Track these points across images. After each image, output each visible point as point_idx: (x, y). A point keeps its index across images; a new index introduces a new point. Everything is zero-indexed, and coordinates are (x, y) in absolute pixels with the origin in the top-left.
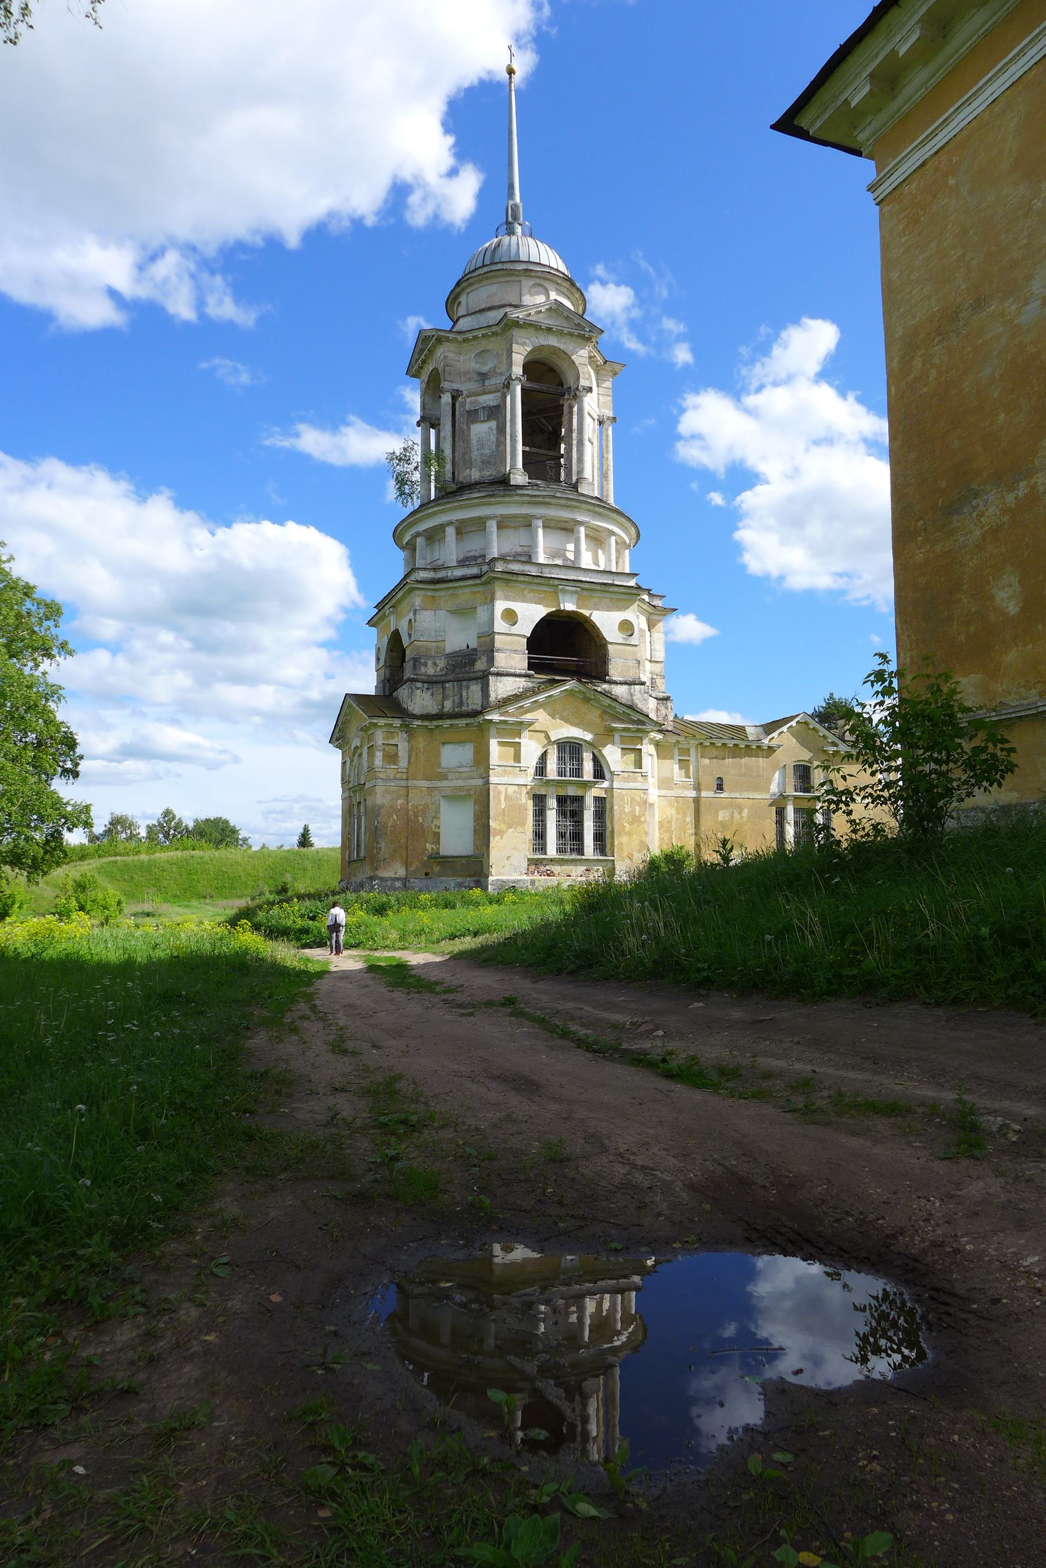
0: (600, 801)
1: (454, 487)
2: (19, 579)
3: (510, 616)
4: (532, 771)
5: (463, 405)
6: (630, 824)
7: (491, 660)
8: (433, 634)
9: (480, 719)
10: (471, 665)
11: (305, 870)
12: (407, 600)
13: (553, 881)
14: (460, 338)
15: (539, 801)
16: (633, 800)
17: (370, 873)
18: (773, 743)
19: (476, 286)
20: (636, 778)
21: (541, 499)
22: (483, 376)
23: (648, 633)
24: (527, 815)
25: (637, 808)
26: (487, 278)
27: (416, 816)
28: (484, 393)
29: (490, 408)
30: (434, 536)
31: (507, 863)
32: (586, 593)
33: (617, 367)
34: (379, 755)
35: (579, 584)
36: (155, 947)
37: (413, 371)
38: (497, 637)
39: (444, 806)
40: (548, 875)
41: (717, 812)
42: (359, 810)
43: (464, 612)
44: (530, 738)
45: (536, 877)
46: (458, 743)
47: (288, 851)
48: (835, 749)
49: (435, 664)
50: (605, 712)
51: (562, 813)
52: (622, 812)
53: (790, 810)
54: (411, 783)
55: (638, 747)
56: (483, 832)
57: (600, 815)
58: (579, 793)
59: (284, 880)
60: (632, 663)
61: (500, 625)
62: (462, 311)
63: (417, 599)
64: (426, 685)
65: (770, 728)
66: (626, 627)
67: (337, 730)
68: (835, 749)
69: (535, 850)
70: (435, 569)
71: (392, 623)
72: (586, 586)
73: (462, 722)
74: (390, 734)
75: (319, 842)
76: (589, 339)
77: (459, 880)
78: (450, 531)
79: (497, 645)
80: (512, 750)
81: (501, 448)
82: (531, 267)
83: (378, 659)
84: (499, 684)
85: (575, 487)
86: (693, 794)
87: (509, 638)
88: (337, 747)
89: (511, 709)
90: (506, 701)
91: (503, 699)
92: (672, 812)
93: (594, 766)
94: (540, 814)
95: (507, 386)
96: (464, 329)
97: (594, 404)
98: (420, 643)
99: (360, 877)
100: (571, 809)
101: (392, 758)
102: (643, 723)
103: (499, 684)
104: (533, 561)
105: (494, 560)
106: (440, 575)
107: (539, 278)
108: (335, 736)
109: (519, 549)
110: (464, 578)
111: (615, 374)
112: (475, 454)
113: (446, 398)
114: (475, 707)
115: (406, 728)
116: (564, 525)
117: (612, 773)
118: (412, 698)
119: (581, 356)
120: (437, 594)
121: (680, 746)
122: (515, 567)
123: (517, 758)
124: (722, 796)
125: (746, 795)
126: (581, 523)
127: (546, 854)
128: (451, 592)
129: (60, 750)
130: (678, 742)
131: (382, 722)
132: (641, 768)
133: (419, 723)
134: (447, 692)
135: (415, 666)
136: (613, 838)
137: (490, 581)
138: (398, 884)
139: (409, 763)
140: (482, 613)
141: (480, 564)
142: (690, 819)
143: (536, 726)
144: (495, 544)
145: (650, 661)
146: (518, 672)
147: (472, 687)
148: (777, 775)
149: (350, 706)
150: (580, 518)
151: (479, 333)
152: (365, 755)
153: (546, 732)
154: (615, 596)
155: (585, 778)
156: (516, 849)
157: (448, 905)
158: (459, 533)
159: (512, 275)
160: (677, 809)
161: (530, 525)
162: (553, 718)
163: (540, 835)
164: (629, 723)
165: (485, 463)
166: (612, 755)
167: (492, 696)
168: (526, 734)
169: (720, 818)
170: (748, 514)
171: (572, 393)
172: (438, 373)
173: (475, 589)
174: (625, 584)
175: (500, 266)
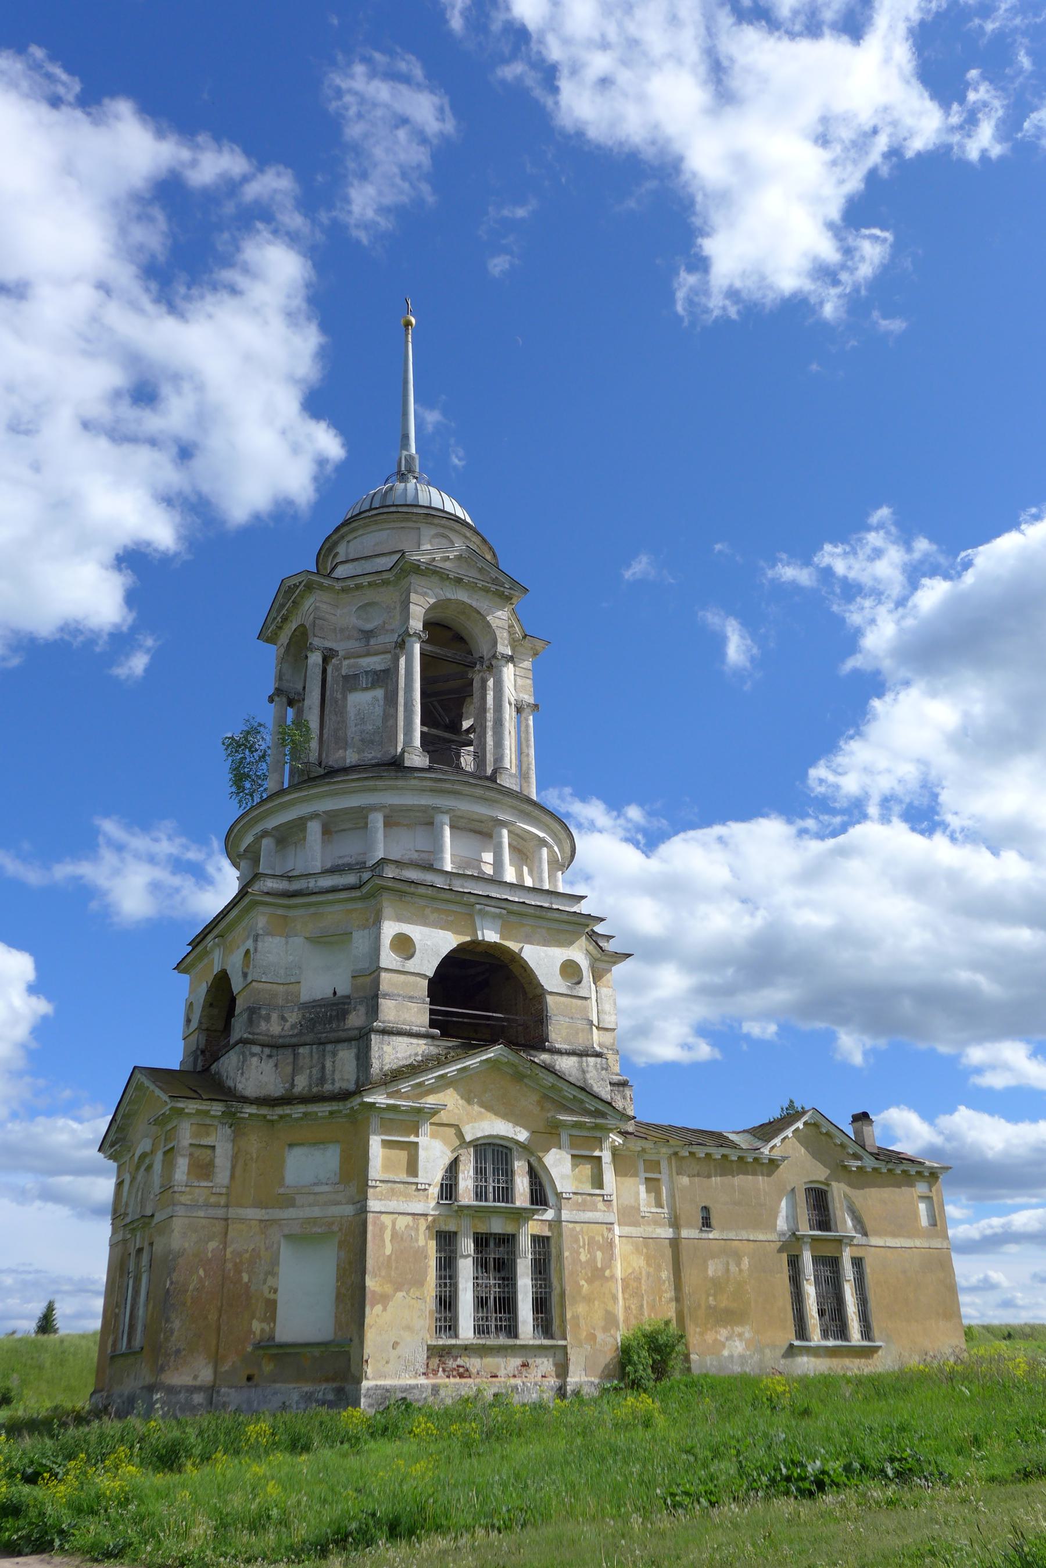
0: (540, 1242)
1: (322, 771)
3: (404, 945)
4: (434, 1191)
5: (338, 668)
6: (590, 1281)
7: (374, 1010)
8: (282, 972)
9: (355, 1102)
10: (343, 1020)
11: (41, 1368)
12: (244, 924)
13: (467, 1387)
14: (338, 586)
15: (446, 1240)
16: (592, 1242)
17: (147, 1377)
18: (776, 1154)
19: (360, 532)
20: (595, 1204)
21: (448, 786)
22: (367, 635)
23: (593, 986)
24: (427, 1267)
25: (599, 1254)
26: (376, 522)
27: (238, 1272)
28: (368, 654)
30: (288, 836)
31: (394, 1354)
32: (513, 918)
33: (539, 645)
34: (182, 1164)
35: (504, 904)
38: (383, 975)
39: (286, 1253)
40: (461, 1376)
41: (705, 1262)
42: (138, 1264)
43: (330, 940)
44: (433, 1136)
45: (441, 1379)
47: (20, 1340)
48: (859, 1163)
49: (283, 1019)
50: (545, 1097)
51: (481, 1265)
52: (576, 1260)
53: (807, 1257)
54: (233, 1212)
55: (597, 1153)
56: (352, 1299)
57: (541, 1268)
58: (509, 1229)
59: (9, 1384)
60: (581, 1024)
61: (388, 958)
63: (261, 920)
64: (267, 1051)
65: (767, 1131)
66: (570, 970)
67: (114, 1128)
68: (859, 1163)
69: (439, 1330)
70: (290, 878)
72: (515, 908)
73: (322, 1109)
74: (205, 1128)
75: (65, 1326)
76: (508, 599)
77: (307, 1388)
78: (314, 828)
79: (384, 987)
80: (403, 1155)
81: (391, 723)
83: (188, 1021)
84: (386, 1048)
85: (493, 778)
86: (668, 1233)
87: (402, 977)
88: (111, 1157)
89: (405, 1087)
90: (397, 1075)
91: (392, 1071)
92: (639, 1262)
93: (531, 1184)
94: (447, 1266)
95: (401, 645)
98: (261, 986)
99: (130, 1385)
100: (496, 1255)
101: (203, 1169)
102: (603, 1115)
103: (386, 1048)
104: (436, 866)
106: (296, 886)
107: (443, 527)
110: (334, 890)
111: (536, 654)
113: (315, 659)
114: (345, 1085)
115: (231, 1119)
116: (477, 826)
117: (559, 1195)
119: (500, 618)
120: (292, 913)
121: (647, 1157)
123: (412, 1168)
124: (711, 1236)
125: (744, 1235)
126: (503, 824)
127: (456, 1336)
128: (312, 910)
130: (644, 1150)
131: (191, 1106)
132: (601, 1187)
133: (252, 1110)
134: (301, 1062)
135: (250, 1021)
136: (563, 1306)
138: (198, 1398)
139: (232, 1177)
140: (360, 942)
142: (666, 1274)
143: (443, 1117)
146: (415, 1029)
148: (783, 1203)
149: (140, 1087)
150: (501, 817)
152: (158, 1167)
153: (457, 1127)
154: (555, 925)
155: (518, 1204)
156: (408, 1328)
157: (298, 1445)
160: (648, 1259)
161: (432, 824)
162: (469, 1101)
163: (447, 1303)
164: (582, 1114)
165: (367, 742)
166: (559, 1164)
167: (376, 1064)
168: (426, 1128)
169: (710, 1273)
171: (487, 663)
173: (350, 906)
174: (567, 909)
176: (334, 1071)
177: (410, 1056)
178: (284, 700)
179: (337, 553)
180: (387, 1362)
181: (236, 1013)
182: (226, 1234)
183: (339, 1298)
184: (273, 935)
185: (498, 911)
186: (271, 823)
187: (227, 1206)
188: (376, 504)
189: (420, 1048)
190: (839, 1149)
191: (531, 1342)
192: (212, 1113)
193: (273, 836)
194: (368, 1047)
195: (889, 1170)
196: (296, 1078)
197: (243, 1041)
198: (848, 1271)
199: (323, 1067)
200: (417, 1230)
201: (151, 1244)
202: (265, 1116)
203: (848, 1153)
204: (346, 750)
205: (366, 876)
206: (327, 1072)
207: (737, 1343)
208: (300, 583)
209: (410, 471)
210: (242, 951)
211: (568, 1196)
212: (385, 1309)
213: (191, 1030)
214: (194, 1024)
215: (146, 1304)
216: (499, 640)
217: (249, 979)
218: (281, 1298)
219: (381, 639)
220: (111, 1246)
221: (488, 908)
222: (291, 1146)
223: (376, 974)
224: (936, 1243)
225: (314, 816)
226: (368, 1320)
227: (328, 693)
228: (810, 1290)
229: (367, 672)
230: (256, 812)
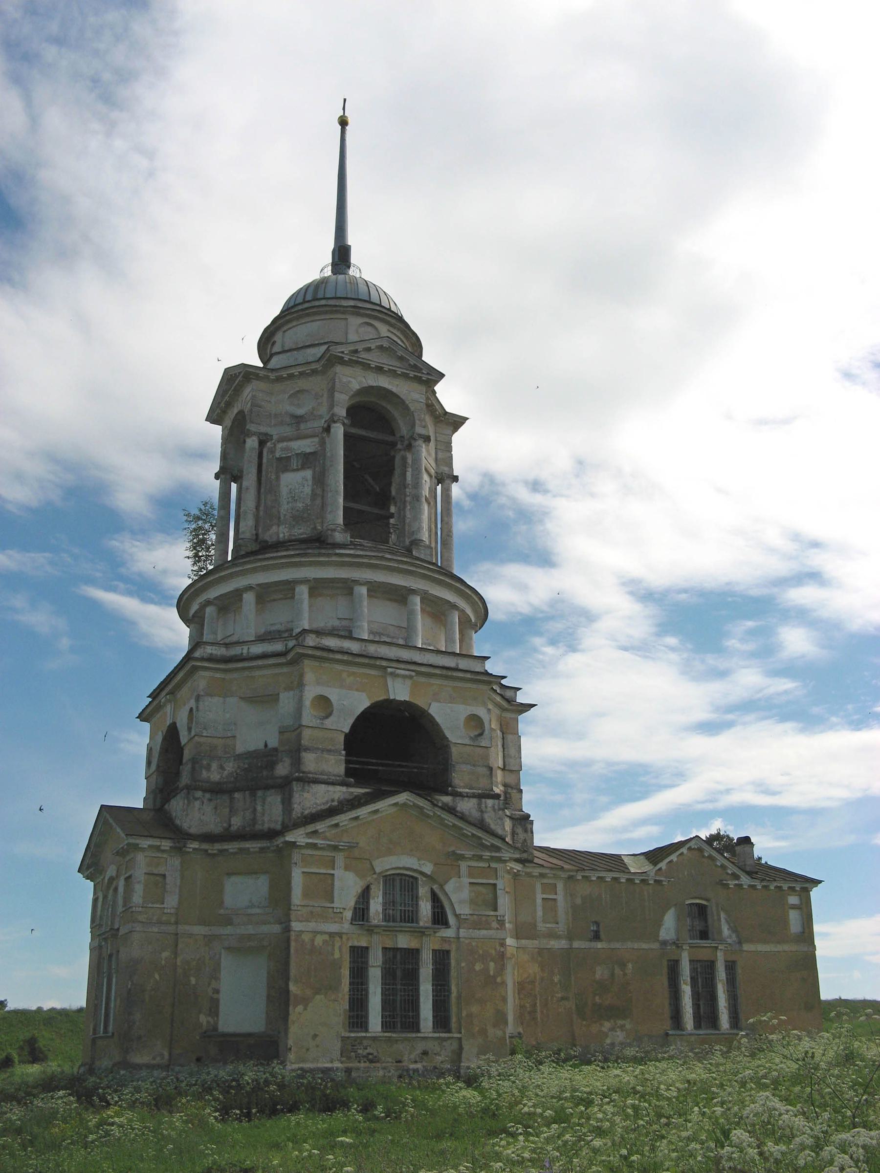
4: (349, 914)
5: (272, 451)
7: (297, 762)
9: (279, 841)
12: (189, 684)
14: (272, 376)
19: (294, 323)
22: (299, 420)
26: (308, 315)
30: (228, 605)
32: (422, 679)
39: (227, 962)
40: (371, 1061)
49: (222, 768)
54: (182, 928)
56: (280, 1001)
58: (414, 944)
60: (482, 770)
61: (309, 717)
62: (277, 349)
63: (202, 680)
64: (208, 796)
70: (227, 645)
71: (167, 715)
78: (249, 598)
82: (360, 304)
83: (149, 763)
84: (306, 795)
92: (534, 969)
93: (433, 907)
96: (278, 367)
100: (402, 968)
104: (355, 636)
105: (304, 631)
108: (87, 861)
109: (337, 623)
110: (264, 656)
112: (285, 507)
113: (252, 443)
114: (272, 826)
115: (179, 850)
120: (228, 676)
122: (331, 642)
126: (413, 592)
127: (367, 1031)
128: (246, 673)
131: (145, 843)
132: (496, 910)
133: (195, 845)
135: (193, 768)
137: (296, 661)
140: (286, 701)
141: (286, 639)
144: (306, 615)
145: (503, 769)
147: (269, 799)
149: (106, 822)
151: (295, 371)
155: (421, 924)
158: (261, 600)
159: (337, 312)
165: (298, 518)
166: (459, 895)
169: (597, 976)
170: (624, 584)
172: (244, 417)
173: (277, 671)
175: (323, 302)
176: (263, 815)
177: (327, 802)
178: (228, 476)
179: (274, 343)
180: (308, 1050)
181: (184, 761)
182: (177, 945)
184: (211, 696)
185: (407, 673)
186: (214, 593)
187: (176, 923)
188: (309, 297)
189: (339, 793)
190: (720, 869)
191: (431, 1035)
192: (162, 848)
193: (215, 605)
194: (291, 796)
195: (764, 887)
196: (232, 819)
197: (188, 787)
198: (721, 974)
199: (255, 810)
200: (334, 946)
202: (206, 851)
203: (728, 874)
204: (279, 526)
205: (291, 644)
206: (258, 814)
207: (619, 1033)
208: (240, 373)
210: (187, 708)
211: (465, 917)
212: (305, 1009)
213: (151, 772)
214: (154, 767)
215: (115, 1000)
216: (417, 422)
217: (193, 733)
219: (309, 425)
220: (91, 950)
221: (398, 671)
222: (230, 874)
223: (299, 731)
225: (249, 588)
226: (292, 1017)
227: (264, 473)
228: (686, 990)
229: (297, 454)
230: (200, 584)
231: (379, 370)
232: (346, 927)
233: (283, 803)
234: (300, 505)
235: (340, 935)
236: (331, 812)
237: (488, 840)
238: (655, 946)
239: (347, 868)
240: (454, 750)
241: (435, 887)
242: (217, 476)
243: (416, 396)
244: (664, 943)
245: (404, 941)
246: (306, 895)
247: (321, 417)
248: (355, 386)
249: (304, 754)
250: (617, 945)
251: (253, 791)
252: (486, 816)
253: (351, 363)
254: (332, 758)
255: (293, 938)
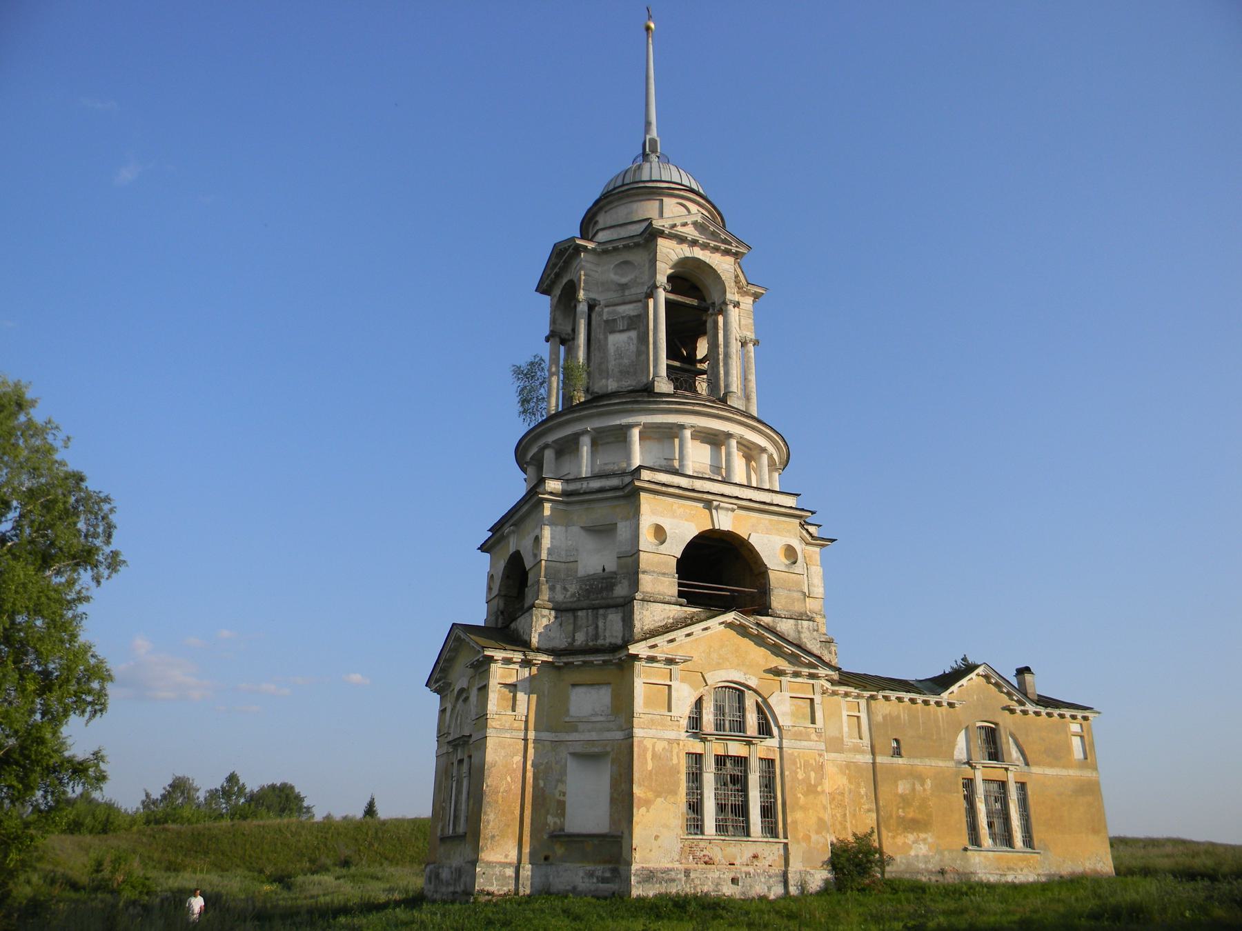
2: (86, 649)
4: (684, 722)
5: (600, 314)
6: (806, 794)
7: (635, 584)
8: (563, 553)
9: (622, 655)
16: (806, 764)
22: (623, 287)
25: (813, 774)
26: (628, 196)
28: (624, 303)
29: (630, 318)
30: (567, 448)
36: (942, 872)
37: (544, 288)
39: (572, 765)
40: (706, 863)
41: (896, 782)
42: (459, 770)
46: (592, 685)
49: (565, 589)
56: (623, 803)
57: (768, 785)
61: (646, 539)
73: (598, 659)
79: (642, 566)
81: (643, 357)
83: (490, 589)
90: (654, 633)
92: (842, 781)
94: (695, 777)
95: (651, 293)
97: (739, 320)
108: (436, 676)
110: (601, 490)
112: (612, 364)
114: (613, 641)
118: (552, 615)
129: (81, 685)
134: (579, 623)
140: (623, 529)
146: (667, 598)
147: (610, 617)
151: (620, 245)
155: (749, 733)
156: (665, 826)
158: (594, 444)
163: (695, 807)
165: (624, 373)
166: (783, 706)
167: (638, 625)
183: (613, 801)
186: (550, 439)
194: (632, 612)
199: (597, 627)
201: (470, 757)
207: (922, 846)
209: (654, 151)
218: (569, 800)
219: (633, 291)
222: (574, 685)
224: (1088, 774)
228: (981, 807)
231: (694, 243)
232: (683, 735)
233: (624, 620)
234: (626, 361)
235: (677, 741)
236: (667, 629)
237: (807, 659)
238: (951, 764)
239: (682, 681)
240: (772, 575)
241: (760, 700)
242: (547, 340)
243: (726, 266)
244: (959, 762)
245: (736, 749)
246: (646, 704)
247: (643, 284)
248: (675, 258)
249: (641, 576)
250: (917, 762)
251: (595, 608)
252: (802, 636)
253: (671, 236)
254: (666, 580)
255: (635, 744)
